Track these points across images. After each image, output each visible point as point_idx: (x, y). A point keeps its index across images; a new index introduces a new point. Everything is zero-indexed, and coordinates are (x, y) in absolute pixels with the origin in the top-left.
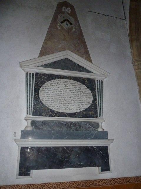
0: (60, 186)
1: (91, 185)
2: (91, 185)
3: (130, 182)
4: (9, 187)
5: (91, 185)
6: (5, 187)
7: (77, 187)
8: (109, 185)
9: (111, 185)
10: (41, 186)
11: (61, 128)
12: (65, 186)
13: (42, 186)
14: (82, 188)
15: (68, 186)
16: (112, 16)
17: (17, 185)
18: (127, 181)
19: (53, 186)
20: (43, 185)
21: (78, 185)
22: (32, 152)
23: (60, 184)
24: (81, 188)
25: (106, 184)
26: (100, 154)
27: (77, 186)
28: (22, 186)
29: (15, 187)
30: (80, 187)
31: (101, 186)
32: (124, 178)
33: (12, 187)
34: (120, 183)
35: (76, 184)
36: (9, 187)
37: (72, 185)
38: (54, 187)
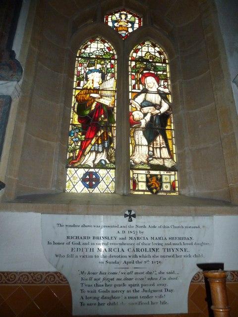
0: (28, 278)
1: (63, 281)
2: (35, 282)
5: (35, 282)
6: (15, 274)
7: (59, 283)
8: (59, 284)
12: (11, 278)
14: (44, 285)
15: (43, 280)
18: (9, 280)
19: (42, 278)
20: (51, 275)
21: (35, 280)
22: (106, 120)
23: (55, 275)
24: (41, 285)
25: (199, 280)
26: (7, 78)
27: (7, 281)
31: (4, 285)
32: (30, 273)
33: (53, 275)
34: (46, 282)
35: (6, 277)
36: (48, 274)
37: (50, 279)
38: (45, 280)
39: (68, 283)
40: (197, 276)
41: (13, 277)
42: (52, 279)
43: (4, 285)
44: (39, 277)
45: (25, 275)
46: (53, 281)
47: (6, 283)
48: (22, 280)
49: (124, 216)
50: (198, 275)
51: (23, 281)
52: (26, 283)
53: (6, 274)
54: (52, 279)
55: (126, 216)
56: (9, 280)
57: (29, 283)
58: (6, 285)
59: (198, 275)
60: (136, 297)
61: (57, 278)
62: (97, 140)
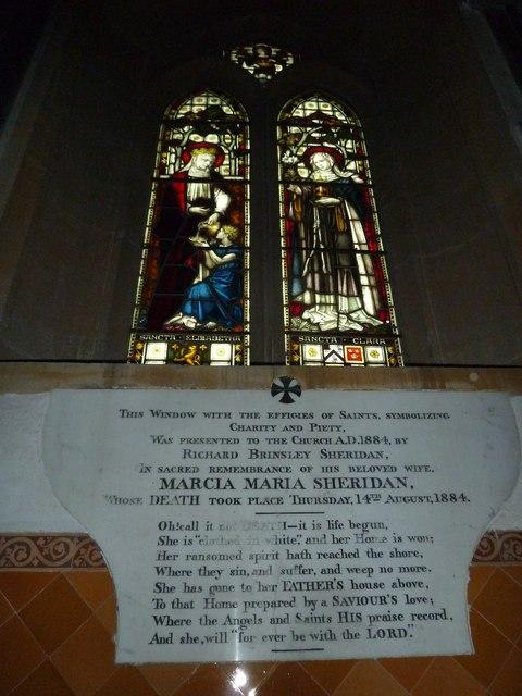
0: (29, 553)
2: (46, 562)
3: (497, 559)
4: (10, 542)
5: (46, 562)
6: (68, 541)
8: (40, 570)
9: (92, 570)
10: (12, 547)
11: (133, 376)
12: (56, 553)
13: (17, 548)
16: (499, 364)
17: (45, 538)
25: (27, 562)
27: (42, 559)
28: (68, 541)
29: (38, 546)
30: (59, 563)
31: (36, 570)
32: (35, 538)
35: (41, 550)
36: (10, 542)
37: (16, 555)
39: (104, 565)
40: (485, 544)
41: (61, 548)
42: (23, 555)
43: (36, 570)
44: (61, 548)
45: (19, 544)
46: (23, 560)
47: (41, 565)
48: (86, 557)
49: (269, 393)
50: (490, 541)
51: (14, 561)
52: (94, 564)
53: (41, 542)
54: (23, 555)
55: (275, 390)
56: (48, 557)
57: (31, 565)
58: (40, 570)
59: (490, 541)
60: (403, 569)
61: (35, 551)
62: (315, 140)
